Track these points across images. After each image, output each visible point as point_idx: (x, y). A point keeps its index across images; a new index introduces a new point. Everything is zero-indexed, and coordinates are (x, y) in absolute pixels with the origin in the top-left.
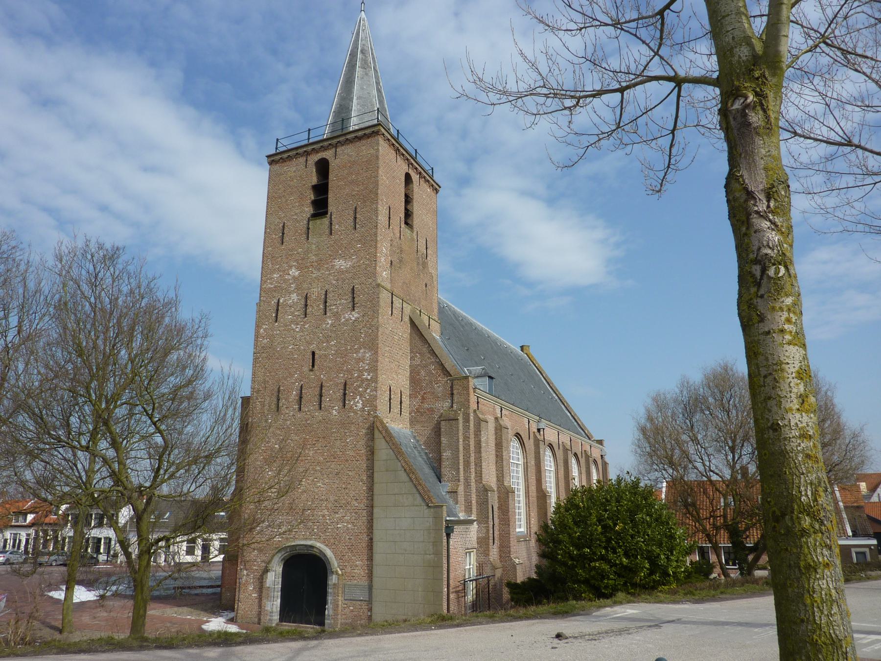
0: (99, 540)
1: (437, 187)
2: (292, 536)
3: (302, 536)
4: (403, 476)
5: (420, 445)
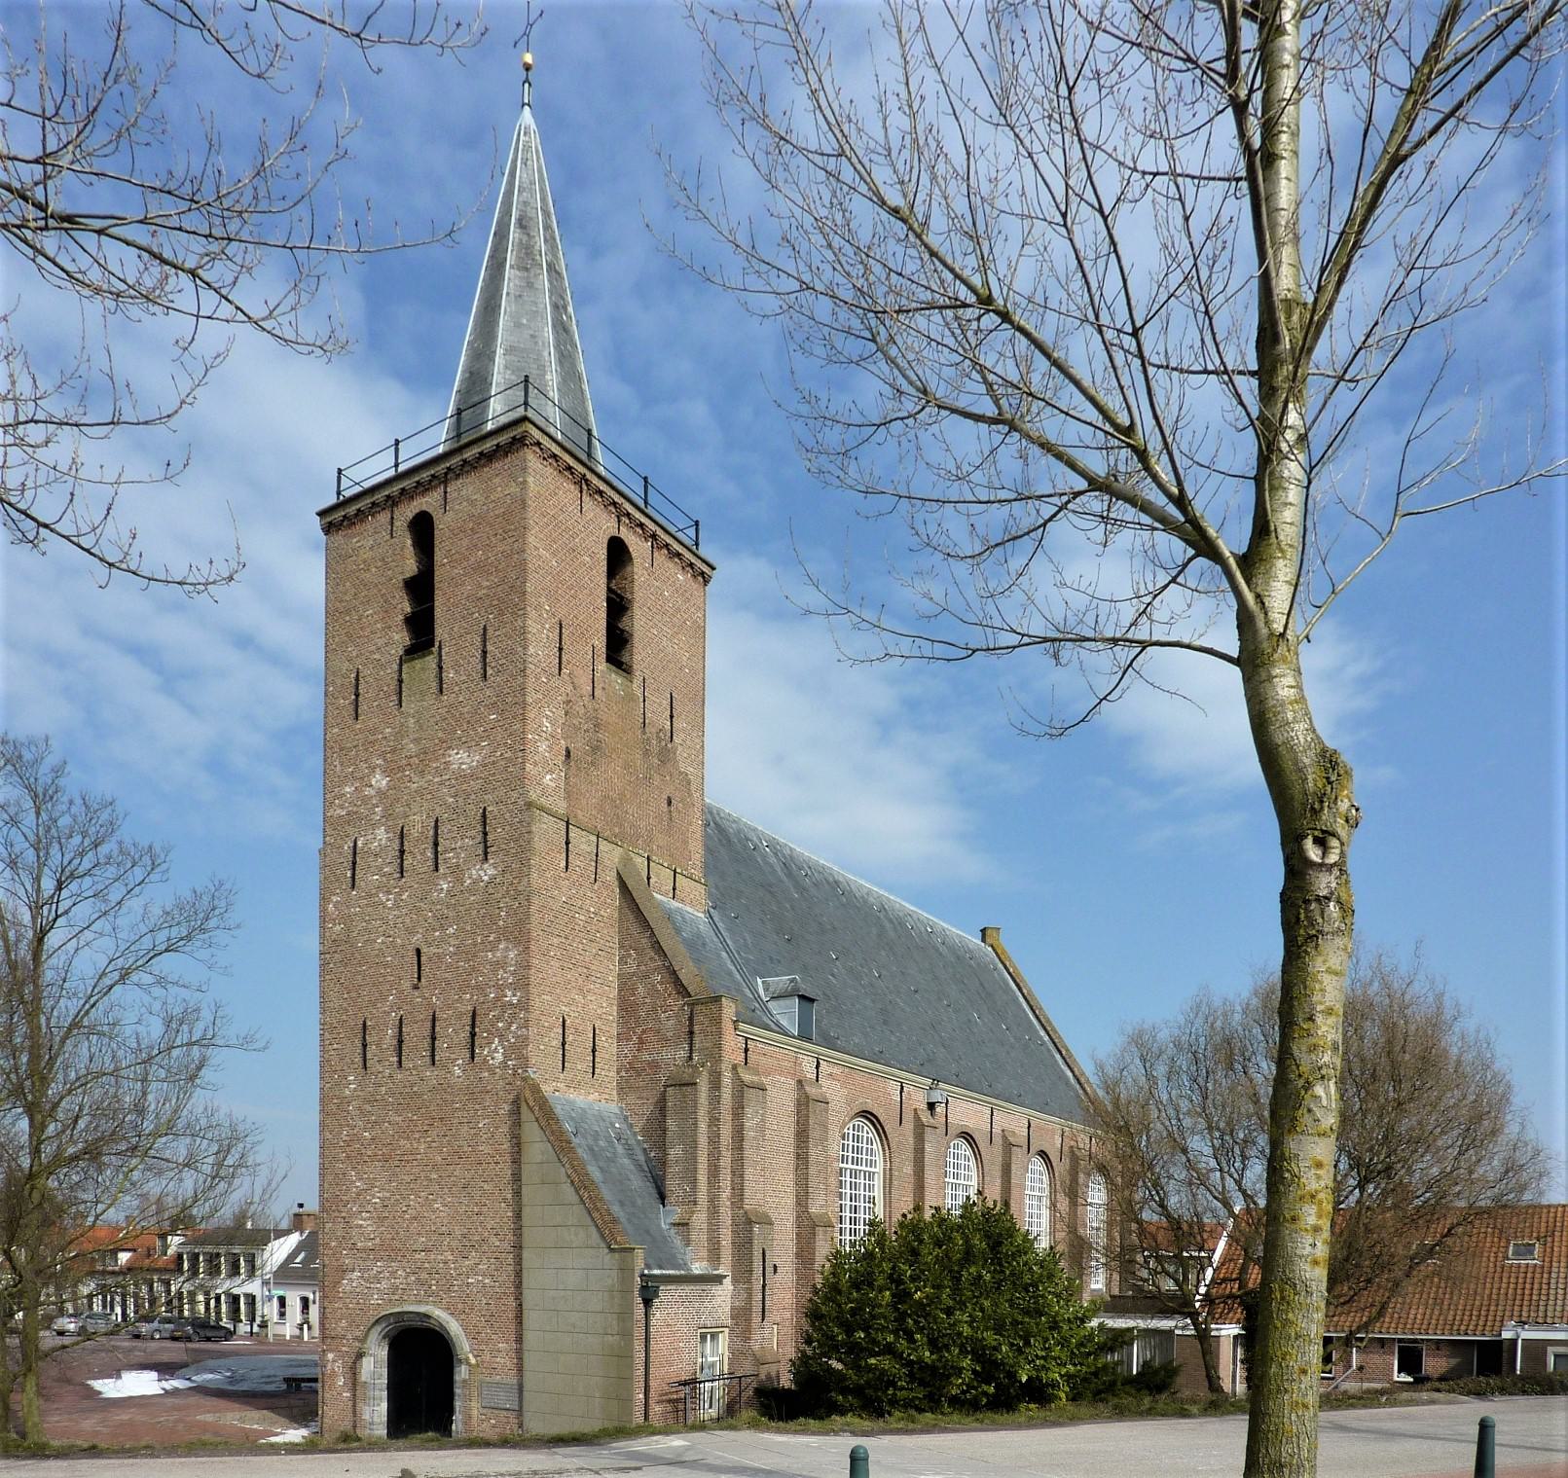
1: (705, 569)
2: (397, 1297)
3: (413, 1298)
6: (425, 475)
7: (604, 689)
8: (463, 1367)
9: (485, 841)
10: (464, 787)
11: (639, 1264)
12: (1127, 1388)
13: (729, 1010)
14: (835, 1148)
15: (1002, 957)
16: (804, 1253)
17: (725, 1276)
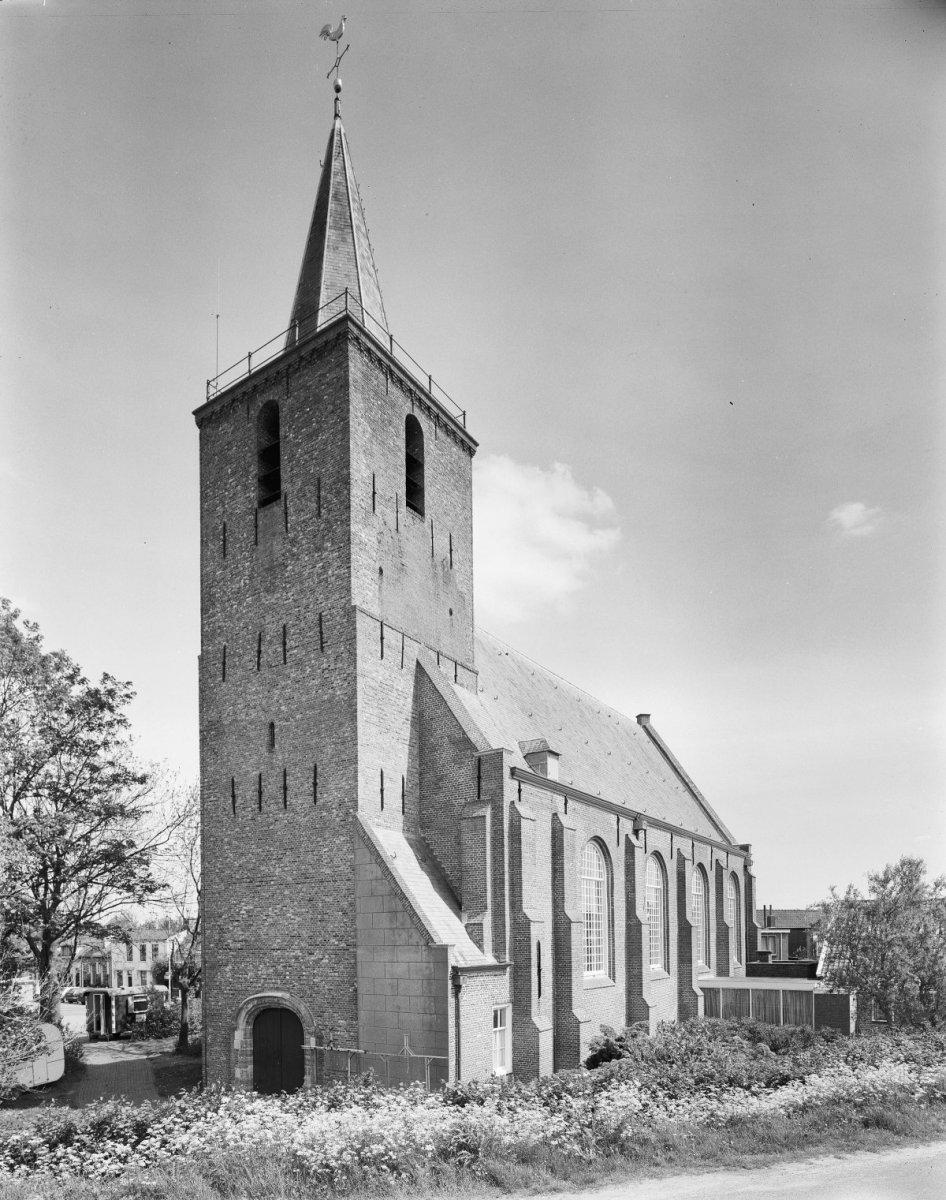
0: (78, 985)
9: (322, 638)
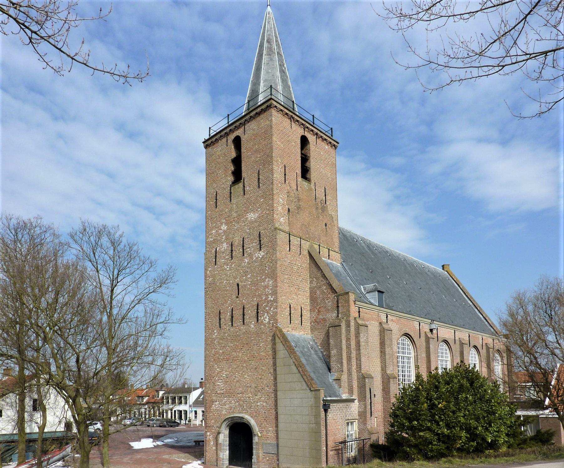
0: (181, 412)
1: (335, 143)
2: (232, 411)
4: (294, 369)
5: (318, 346)
6: (238, 124)
7: (301, 187)
8: (256, 437)
9: (260, 243)
10: (253, 225)
11: (322, 396)
12: (533, 442)
13: (352, 297)
14: (395, 348)
15: (451, 275)
16: (386, 390)
17: (355, 399)
